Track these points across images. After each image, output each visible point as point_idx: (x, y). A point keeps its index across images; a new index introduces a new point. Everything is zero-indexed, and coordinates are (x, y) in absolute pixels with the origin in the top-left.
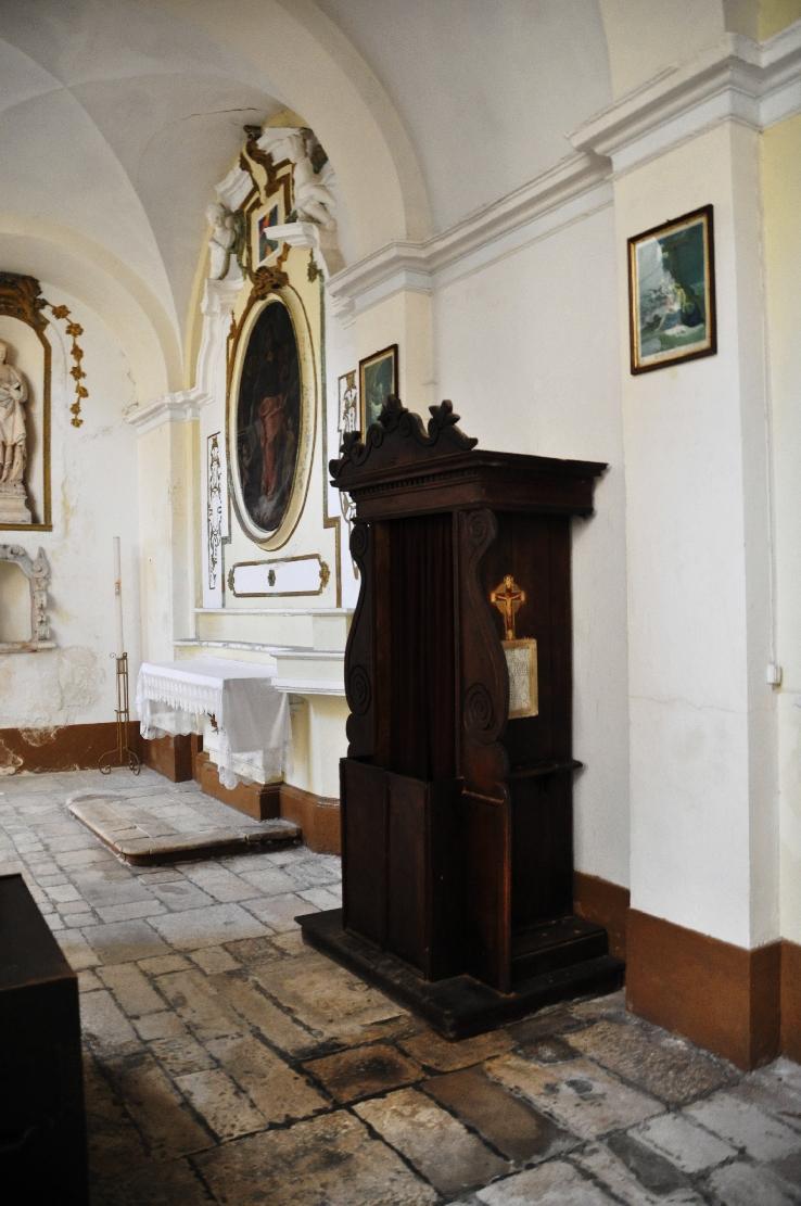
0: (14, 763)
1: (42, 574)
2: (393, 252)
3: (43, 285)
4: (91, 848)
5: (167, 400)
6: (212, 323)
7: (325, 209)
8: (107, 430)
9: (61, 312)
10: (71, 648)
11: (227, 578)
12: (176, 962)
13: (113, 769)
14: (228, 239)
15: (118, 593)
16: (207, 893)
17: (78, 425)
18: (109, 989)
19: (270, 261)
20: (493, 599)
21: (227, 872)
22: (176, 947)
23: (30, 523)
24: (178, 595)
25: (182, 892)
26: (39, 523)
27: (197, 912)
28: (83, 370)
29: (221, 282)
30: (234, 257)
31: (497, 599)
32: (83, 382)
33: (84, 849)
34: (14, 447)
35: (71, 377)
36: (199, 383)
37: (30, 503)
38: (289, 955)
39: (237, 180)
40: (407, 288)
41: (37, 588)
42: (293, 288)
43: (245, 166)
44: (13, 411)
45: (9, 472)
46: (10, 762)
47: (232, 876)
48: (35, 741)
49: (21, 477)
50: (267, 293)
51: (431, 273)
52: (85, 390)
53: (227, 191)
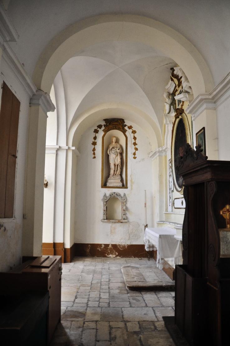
0: (115, 254)
1: (125, 200)
2: (200, 98)
3: (125, 121)
4: (121, 283)
5: (157, 150)
6: (168, 127)
7: (191, 88)
8: (143, 159)
9: (130, 127)
10: (132, 222)
11: (173, 203)
12: (121, 325)
13: (142, 258)
14: (170, 102)
15: (145, 207)
16: (145, 302)
17: (135, 159)
18: (97, 329)
19: (180, 107)
20: (221, 213)
21: (156, 296)
22: (124, 319)
23: (121, 186)
24: (161, 207)
25: (138, 301)
26: (124, 186)
27: (138, 309)
28: (136, 143)
29: (169, 114)
30: (172, 107)
31: (223, 213)
32: (136, 146)
33: (119, 282)
34: (118, 165)
35: (133, 145)
36: (165, 145)
37: (122, 180)
38: (157, 330)
39: (171, 84)
40: (206, 109)
41: (123, 204)
42: (185, 114)
43: (172, 80)
44: (117, 155)
45: (116, 172)
46: (114, 254)
47: (157, 297)
48: (121, 248)
49: (120, 173)
50: (179, 116)
51: (215, 102)
52: (137, 148)
53: (169, 88)
